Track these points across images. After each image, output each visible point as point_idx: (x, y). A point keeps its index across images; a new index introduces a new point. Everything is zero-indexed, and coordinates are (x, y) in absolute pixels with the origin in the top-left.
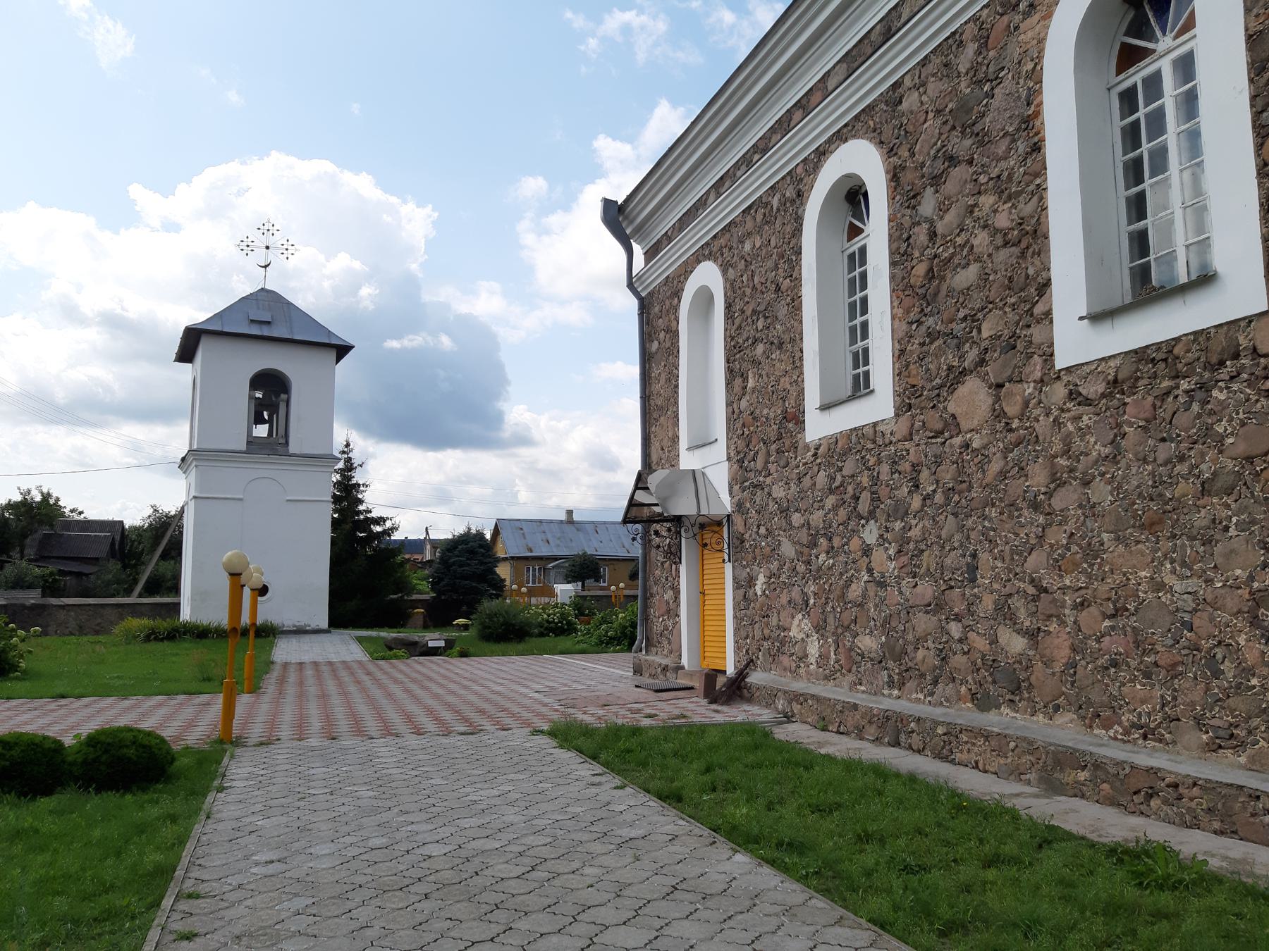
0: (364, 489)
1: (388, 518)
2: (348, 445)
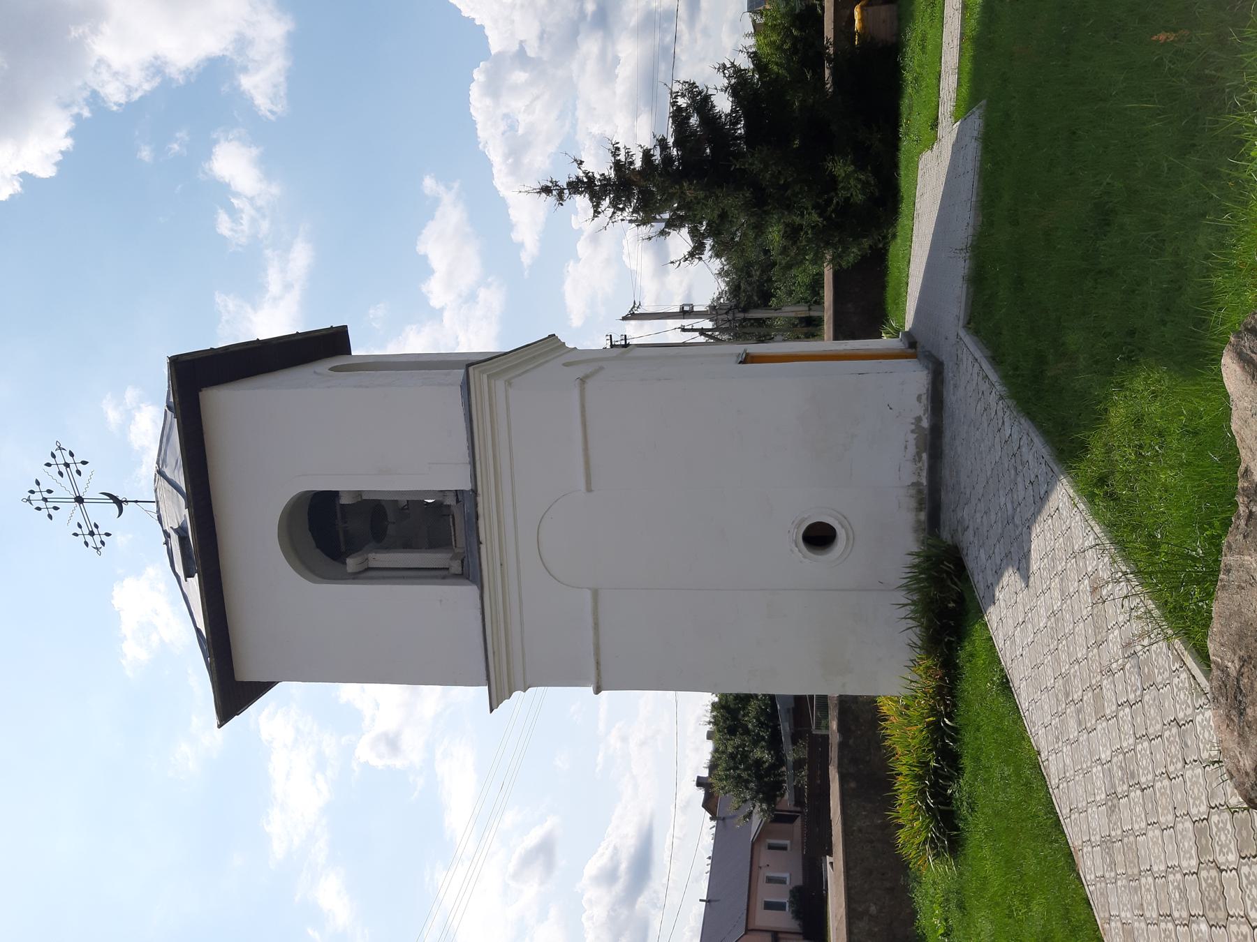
0: (622, 152)
1: (674, 104)
2: (546, 190)
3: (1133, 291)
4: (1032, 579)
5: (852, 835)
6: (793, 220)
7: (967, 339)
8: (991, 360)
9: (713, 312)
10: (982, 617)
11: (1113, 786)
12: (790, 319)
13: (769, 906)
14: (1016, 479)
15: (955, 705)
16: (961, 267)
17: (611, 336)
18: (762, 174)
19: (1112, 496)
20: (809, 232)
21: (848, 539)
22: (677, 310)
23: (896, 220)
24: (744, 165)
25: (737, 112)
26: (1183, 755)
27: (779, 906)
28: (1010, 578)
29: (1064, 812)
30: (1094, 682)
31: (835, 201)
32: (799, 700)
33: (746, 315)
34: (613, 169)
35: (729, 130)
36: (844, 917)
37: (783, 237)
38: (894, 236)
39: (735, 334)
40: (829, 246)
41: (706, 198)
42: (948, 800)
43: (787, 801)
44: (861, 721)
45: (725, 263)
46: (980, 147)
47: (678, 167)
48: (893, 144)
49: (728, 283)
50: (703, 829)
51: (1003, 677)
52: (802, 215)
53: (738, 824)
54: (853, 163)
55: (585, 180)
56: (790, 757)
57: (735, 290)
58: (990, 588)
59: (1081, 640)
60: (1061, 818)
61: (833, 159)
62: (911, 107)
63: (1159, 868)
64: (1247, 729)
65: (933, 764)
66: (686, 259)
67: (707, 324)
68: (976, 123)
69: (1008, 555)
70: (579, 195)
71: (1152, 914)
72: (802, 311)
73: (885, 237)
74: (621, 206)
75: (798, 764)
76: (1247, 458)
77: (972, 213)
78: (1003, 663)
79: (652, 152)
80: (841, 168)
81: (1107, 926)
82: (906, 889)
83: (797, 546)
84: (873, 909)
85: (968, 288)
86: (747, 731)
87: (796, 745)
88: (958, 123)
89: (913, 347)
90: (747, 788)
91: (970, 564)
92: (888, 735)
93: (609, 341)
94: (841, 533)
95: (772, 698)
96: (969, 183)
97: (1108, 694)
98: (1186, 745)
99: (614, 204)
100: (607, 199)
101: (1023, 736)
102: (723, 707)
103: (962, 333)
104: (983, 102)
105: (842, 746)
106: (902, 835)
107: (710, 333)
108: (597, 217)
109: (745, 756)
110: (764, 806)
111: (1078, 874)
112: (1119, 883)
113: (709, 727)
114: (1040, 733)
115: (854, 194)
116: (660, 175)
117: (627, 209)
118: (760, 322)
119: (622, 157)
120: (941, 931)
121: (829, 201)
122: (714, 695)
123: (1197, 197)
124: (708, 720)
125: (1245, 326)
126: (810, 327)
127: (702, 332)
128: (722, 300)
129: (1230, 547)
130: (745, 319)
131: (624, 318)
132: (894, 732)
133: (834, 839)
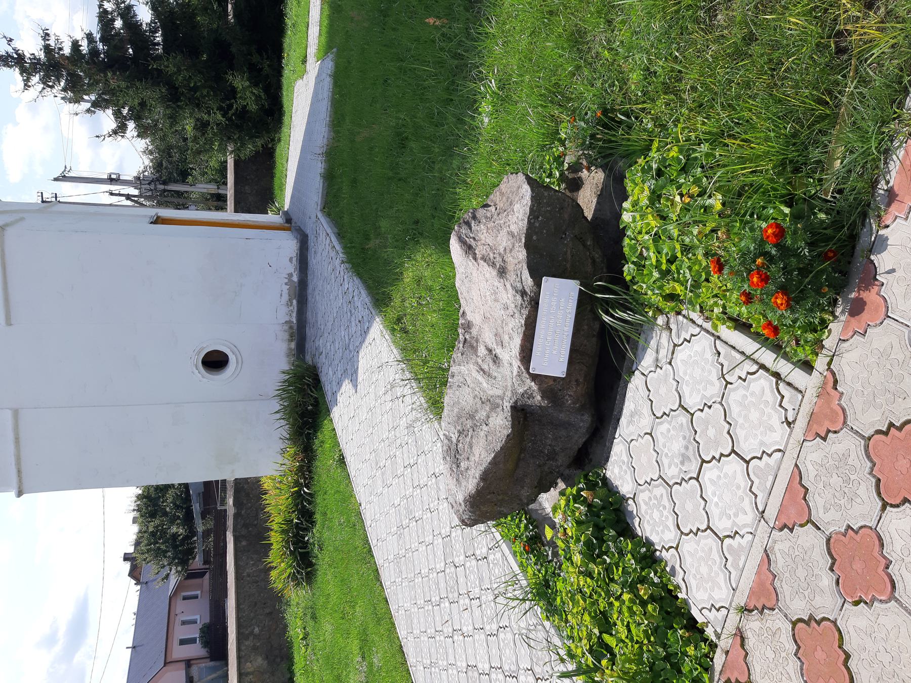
1: (100, 6)
3: (417, 194)
4: (359, 387)
5: (242, 579)
6: (202, 117)
7: (323, 220)
8: (337, 235)
9: (138, 181)
10: (329, 415)
11: (401, 521)
12: (203, 194)
13: (183, 642)
14: (350, 319)
15: (312, 478)
16: (318, 167)
17: (42, 193)
18: (176, 76)
19: (405, 331)
20: (215, 128)
21: (237, 362)
22: (106, 177)
23: (281, 128)
24: (160, 66)
25: (156, 23)
26: (438, 496)
27: (192, 641)
28: (346, 386)
29: (374, 542)
30: (392, 453)
31: (235, 107)
32: (207, 484)
33: (166, 187)
34: (42, 51)
35: (149, 36)
36: (235, 640)
37: (194, 128)
38: (279, 140)
39: (158, 202)
40: (231, 141)
41: (127, 88)
42: (305, 545)
43: (197, 562)
44: (251, 496)
45: (149, 144)
46: (332, 82)
47: (104, 59)
48: (278, 71)
49: (152, 161)
50: (131, 592)
51: (340, 455)
52: (209, 114)
53: (157, 585)
54: (248, 80)
55: (15, 56)
56: (200, 528)
57: (158, 166)
58: (334, 394)
59: (386, 427)
60: (372, 547)
61: (233, 74)
62: (290, 46)
63: (425, 571)
64: (460, 475)
65: (295, 521)
66: (110, 136)
67: (134, 192)
68: (330, 64)
69: (345, 371)
70: (8, 68)
71: (421, 602)
72: (212, 188)
73: (273, 140)
74: (50, 84)
75: (206, 534)
76: (464, 305)
77: (327, 128)
78: (341, 446)
79: (80, 43)
80: (239, 82)
81: (396, 614)
82: (280, 612)
83: (197, 369)
84: (257, 630)
85: (324, 183)
86: (165, 514)
87: (204, 519)
88: (319, 62)
89: (289, 223)
90: (165, 557)
91: (323, 379)
92: (268, 504)
93: (40, 197)
94: (232, 358)
95: (186, 486)
96: (325, 107)
97: (399, 460)
98: (439, 489)
99: (44, 81)
100: (37, 76)
101: (352, 495)
102: (145, 497)
103: (320, 215)
104: (335, 50)
105: (236, 516)
106: (273, 574)
107: (136, 199)
108: (26, 89)
109: (163, 532)
110: (179, 568)
111: (381, 582)
112: (404, 584)
113: (135, 514)
114: (361, 493)
115: (249, 103)
116: (87, 63)
117: (56, 87)
118: (179, 194)
119: (52, 42)
120: (301, 637)
121: (230, 107)
122: (139, 488)
123: (453, 135)
124: (132, 508)
125: (463, 220)
126: (218, 202)
127: (128, 197)
128: (146, 173)
129: (454, 361)
130: (165, 191)
131: (56, 179)
132: (272, 502)
133: (229, 584)
